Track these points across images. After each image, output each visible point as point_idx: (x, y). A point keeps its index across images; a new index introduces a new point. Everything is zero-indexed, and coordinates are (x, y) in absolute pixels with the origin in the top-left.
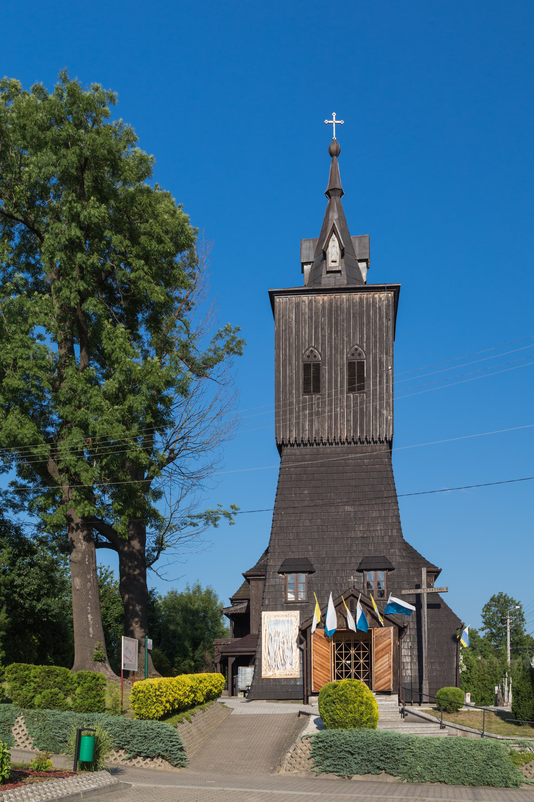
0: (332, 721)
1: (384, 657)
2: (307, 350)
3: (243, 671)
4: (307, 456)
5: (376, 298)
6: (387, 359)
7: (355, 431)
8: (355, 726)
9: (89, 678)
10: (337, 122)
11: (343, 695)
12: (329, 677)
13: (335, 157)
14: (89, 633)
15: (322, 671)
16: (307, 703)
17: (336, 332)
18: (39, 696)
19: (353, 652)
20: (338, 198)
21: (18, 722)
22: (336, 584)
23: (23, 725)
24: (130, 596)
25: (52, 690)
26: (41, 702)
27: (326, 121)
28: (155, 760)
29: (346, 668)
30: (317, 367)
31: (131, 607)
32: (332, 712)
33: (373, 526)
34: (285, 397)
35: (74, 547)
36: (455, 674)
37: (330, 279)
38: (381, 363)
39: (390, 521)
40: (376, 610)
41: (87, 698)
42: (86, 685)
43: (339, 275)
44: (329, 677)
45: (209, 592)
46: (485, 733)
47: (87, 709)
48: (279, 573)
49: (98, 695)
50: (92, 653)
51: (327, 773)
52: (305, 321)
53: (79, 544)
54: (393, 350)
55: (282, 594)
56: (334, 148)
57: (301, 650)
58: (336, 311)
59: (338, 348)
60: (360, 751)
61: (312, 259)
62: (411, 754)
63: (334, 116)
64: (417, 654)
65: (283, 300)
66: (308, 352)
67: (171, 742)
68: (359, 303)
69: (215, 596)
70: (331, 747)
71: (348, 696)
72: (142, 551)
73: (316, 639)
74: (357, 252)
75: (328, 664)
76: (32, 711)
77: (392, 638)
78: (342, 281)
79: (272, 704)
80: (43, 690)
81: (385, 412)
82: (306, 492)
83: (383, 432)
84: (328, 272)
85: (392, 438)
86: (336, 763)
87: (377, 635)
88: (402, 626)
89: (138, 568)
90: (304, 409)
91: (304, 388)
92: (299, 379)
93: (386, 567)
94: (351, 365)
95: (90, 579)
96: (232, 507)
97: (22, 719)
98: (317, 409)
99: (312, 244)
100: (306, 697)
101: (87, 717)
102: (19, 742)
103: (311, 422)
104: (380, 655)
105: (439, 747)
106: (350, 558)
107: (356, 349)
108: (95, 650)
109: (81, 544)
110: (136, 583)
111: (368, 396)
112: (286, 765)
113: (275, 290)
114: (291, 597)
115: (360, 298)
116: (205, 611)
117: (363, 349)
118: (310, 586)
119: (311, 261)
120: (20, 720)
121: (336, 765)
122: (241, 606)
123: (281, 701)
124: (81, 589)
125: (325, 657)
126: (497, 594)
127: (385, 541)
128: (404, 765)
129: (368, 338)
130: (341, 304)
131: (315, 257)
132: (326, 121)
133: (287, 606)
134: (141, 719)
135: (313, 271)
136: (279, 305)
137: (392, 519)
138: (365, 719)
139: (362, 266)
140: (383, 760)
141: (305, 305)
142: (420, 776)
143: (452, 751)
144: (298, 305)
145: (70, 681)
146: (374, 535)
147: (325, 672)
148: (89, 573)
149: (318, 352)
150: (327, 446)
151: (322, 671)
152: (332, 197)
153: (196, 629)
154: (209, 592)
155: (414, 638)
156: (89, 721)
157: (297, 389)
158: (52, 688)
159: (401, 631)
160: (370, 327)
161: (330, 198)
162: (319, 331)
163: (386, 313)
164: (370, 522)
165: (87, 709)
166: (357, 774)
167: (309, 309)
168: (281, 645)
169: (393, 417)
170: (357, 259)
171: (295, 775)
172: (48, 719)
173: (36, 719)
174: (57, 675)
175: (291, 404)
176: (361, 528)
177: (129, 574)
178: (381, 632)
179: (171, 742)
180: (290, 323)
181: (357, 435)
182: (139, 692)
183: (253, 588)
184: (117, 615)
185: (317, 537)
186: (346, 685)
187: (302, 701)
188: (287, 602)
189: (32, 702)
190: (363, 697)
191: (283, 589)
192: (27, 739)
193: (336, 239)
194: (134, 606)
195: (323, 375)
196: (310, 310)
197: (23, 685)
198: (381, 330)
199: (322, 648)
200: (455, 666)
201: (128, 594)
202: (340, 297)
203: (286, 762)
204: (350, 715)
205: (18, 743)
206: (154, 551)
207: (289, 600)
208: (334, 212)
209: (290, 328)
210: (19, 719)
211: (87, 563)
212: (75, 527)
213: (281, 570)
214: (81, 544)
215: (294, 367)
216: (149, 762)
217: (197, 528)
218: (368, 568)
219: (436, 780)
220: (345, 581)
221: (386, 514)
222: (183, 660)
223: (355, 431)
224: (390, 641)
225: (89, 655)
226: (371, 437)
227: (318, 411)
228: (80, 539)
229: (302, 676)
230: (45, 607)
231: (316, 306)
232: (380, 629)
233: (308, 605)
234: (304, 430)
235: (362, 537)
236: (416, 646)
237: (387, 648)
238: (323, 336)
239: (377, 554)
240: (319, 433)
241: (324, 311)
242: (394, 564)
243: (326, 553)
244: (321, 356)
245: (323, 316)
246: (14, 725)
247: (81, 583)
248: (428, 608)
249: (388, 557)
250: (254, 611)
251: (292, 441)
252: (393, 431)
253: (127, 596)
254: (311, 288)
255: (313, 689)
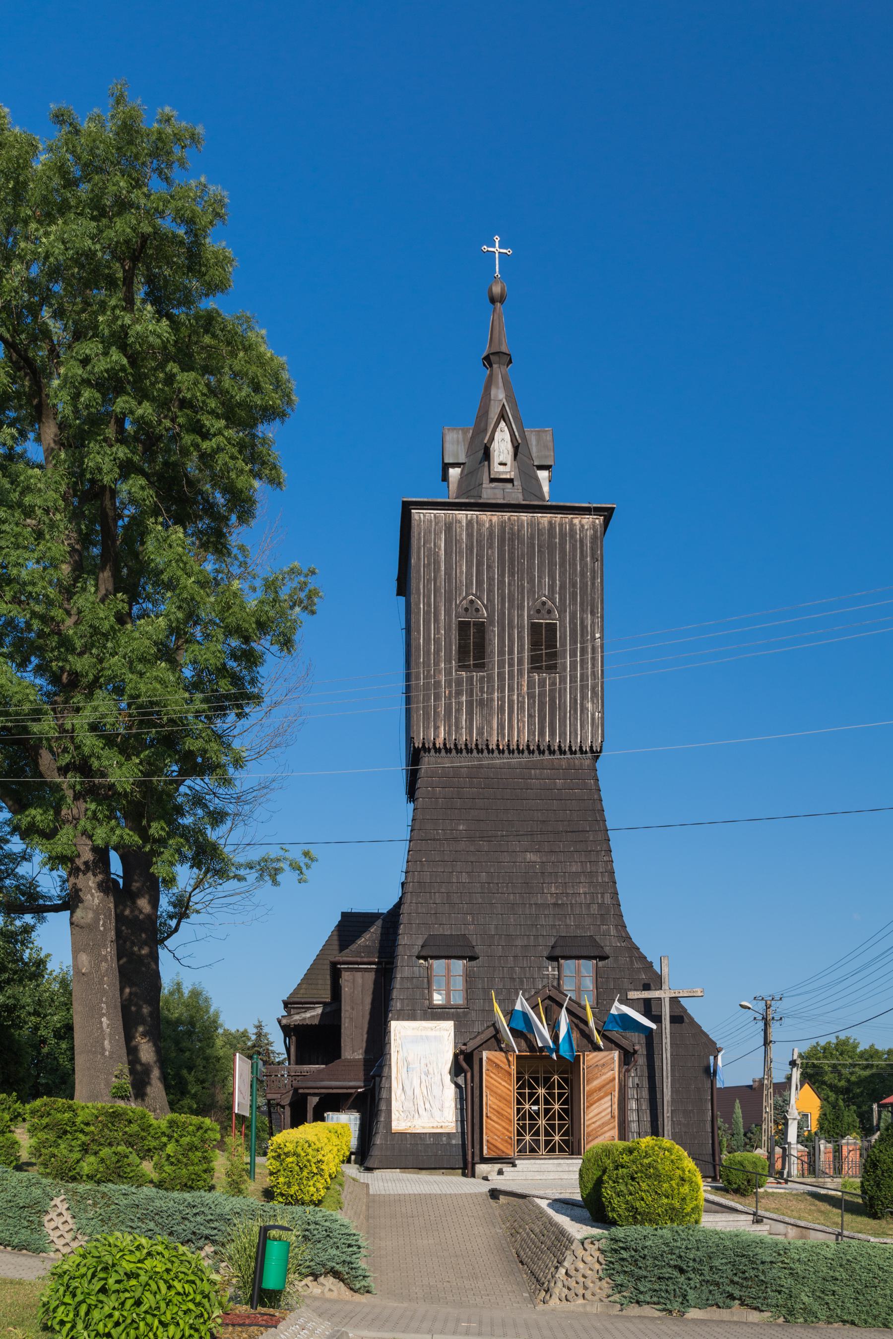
0: (628, 1211)
1: (602, 1101)
2: (465, 598)
3: (335, 1119)
4: (462, 770)
5: (575, 525)
6: (593, 623)
7: (542, 733)
8: (672, 1220)
9: (191, 1128)
10: (502, 251)
11: (650, 1166)
12: (510, 1132)
13: (498, 304)
14: (104, 1049)
15: (500, 1121)
16: (473, 1176)
17: (512, 575)
18: (92, 1159)
19: (541, 1091)
20: (503, 368)
21: (56, 1206)
22: (512, 979)
23: (64, 1212)
24: (134, 989)
25: (119, 1148)
26: (97, 1170)
27: (485, 248)
28: (322, 1279)
29: (532, 1118)
30: (481, 628)
31: (133, 1009)
32: (631, 1194)
33: (573, 887)
34: (429, 671)
35: (81, 901)
36: (710, 1130)
37: (497, 491)
38: (583, 627)
39: (600, 880)
40: (592, 1023)
41: (186, 1165)
42: (185, 1140)
43: (509, 485)
44: (510, 1132)
45: (196, 994)
46: (846, 1233)
47: (186, 1185)
48: (419, 957)
49: (205, 1158)
50: (108, 1083)
51: (641, 1306)
52: (461, 552)
53: (89, 897)
54: (602, 609)
55: (423, 994)
56: (497, 290)
57: (457, 1085)
58: (512, 540)
59: (514, 599)
60: (697, 1266)
61: (462, 459)
62: (787, 1271)
63: (497, 241)
64: (647, 1097)
65: (424, 516)
66: (464, 602)
67: (350, 1246)
68: (549, 531)
69: (207, 1000)
70: (644, 1258)
71: (660, 1167)
72: (154, 917)
73: (490, 1068)
74: (534, 455)
75: (509, 1110)
76: (82, 1188)
77: (617, 1069)
78: (515, 495)
79: (408, 1175)
80: (101, 1147)
81: (590, 705)
82: (461, 827)
83: (587, 737)
84: (493, 480)
85: (601, 747)
86: (656, 1287)
87: (590, 1063)
88: (632, 1051)
89: (146, 944)
90: (459, 693)
91: (459, 659)
92: (451, 645)
93: (596, 954)
94: (535, 628)
95: (105, 956)
96: (306, 854)
97: (62, 1201)
98: (479, 694)
99: (460, 436)
100: (470, 1166)
101: (190, 1200)
102: (59, 1243)
103: (470, 714)
104: (596, 1096)
105: (833, 1260)
106: (536, 937)
107: (544, 603)
108: (114, 1079)
109: (92, 895)
110: (144, 969)
111: (563, 680)
112: (558, 1290)
113: (414, 499)
114: (438, 999)
115: (550, 523)
116: (192, 1023)
117: (554, 603)
118: (469, 978)
119: (461, 461)
120: (59, 1204)
121: (655, 1290)
122: (313, 1014)
123: (424, 1171)
124: (90, 973)
125: (504, 1099)
126: (241, 1030)
127: (592, 912)
128: (776, 1291)
129: (563, 587)
130: (519, 531)
131: (467, 456)
132: (485, 248)
133: (432, 1013)
134: (286, 1204)
135: (463, 477)
136: (419, 525)
137: (603, 876)
138: (688, 1209)
139: (543, 475)
140: (737, 1283)
141: (461, 527)
142: (808, 1311)
143: (857, 1268)
144: (449, 527)
145: (153, 1132)
146: (573, 902)
147: (504, 1124)
148: (105, 947)
149: (483, 603)
150: (495, 755)
151: (500, 1121)
152: (495, 366)
153: (182, 1051)
154: (196, 994)
155: (642, 1071)
156: (194, 1207)
157: (448, 661)
158: (118, 1144)
159: (627, 1057)
160: (566, 570)
161: (491, 366)
162: (483, 570)
163: (592, 549)
164: (567, 880)
165: (186, 1185)
166: (695, 1307)
167: (467, 535)
168: (423, 1077)
169: (603, 714)
170: (536, 464)
171: (581, 1309)
172: (116, 1201)
173: (90, 1202)
174: (130, 1122)
175: (437, 684)
176: (553, 890)
177: (133, 953)
178: (596, 1059)
179: (350, 1246)
180: (437, 554)
181: (544, 740)
182: (287, 1155)
183: (346, 983)
184: (58, 1025)
185: (480, 901)
186: (653, 1148)
187: (460, 1171)
188: (432, 1007)
189: (78, 1170)
190: (684, 1171)
191: (426, 986)
192: (75, 1239)
193: (506, 429)
194: (140, 1008)
195: (490, 640)
196: (470, 535)
197: (60, 1137)
198: (583, 575)
199: (500, 1083)
200: (709, 1118)
201: (130, 987)
202: (518, 519)
203: (560, 1284)
204: (665, 1201)
205: (57, 1247)
206: (171, 917)
207: (435, 1002)
208: (498, 388)
209: (437, 563)
210: (57, 1201)
211: (102, 929)
212: (82, 867)
213: (423, 954)
214: (92, 895)
215: (442, 624)
216: (310, 1284)
217: (243, 884)
218: (567, 954)
219: (837, 1319)
220: (528, 975)
221: (594, 869)
222: (179, 1100)
223: (542, 733)
224: (614, 1074)
225: (102, 1086)
226: (568, 744)
227: (482, 701)
228: (91, 887)
229: (459, 1130)
230: (11, 1002)
231: (479, 530)
232: (595, 1054)
233: (468, 1013)
234: (458, 728)
235: (555, 904)
236: (646, 1084)
237: (608, 1086)
238: (491, 579)
239: (579, 933)
240: (483, 734)
241: (491, 539)
242: (608, 950)
243: (496, 928)
244: (487, 611)
245: (491, 546)
246: (47, 1212)
247: (90, 962)
248: (671, 1022)
249: (597, 938)
250: (347, 1020)
251: (440, 743)
252: (603, 737)
253: (127, 990)
254: (472, 501)
255: (485, 1152)
